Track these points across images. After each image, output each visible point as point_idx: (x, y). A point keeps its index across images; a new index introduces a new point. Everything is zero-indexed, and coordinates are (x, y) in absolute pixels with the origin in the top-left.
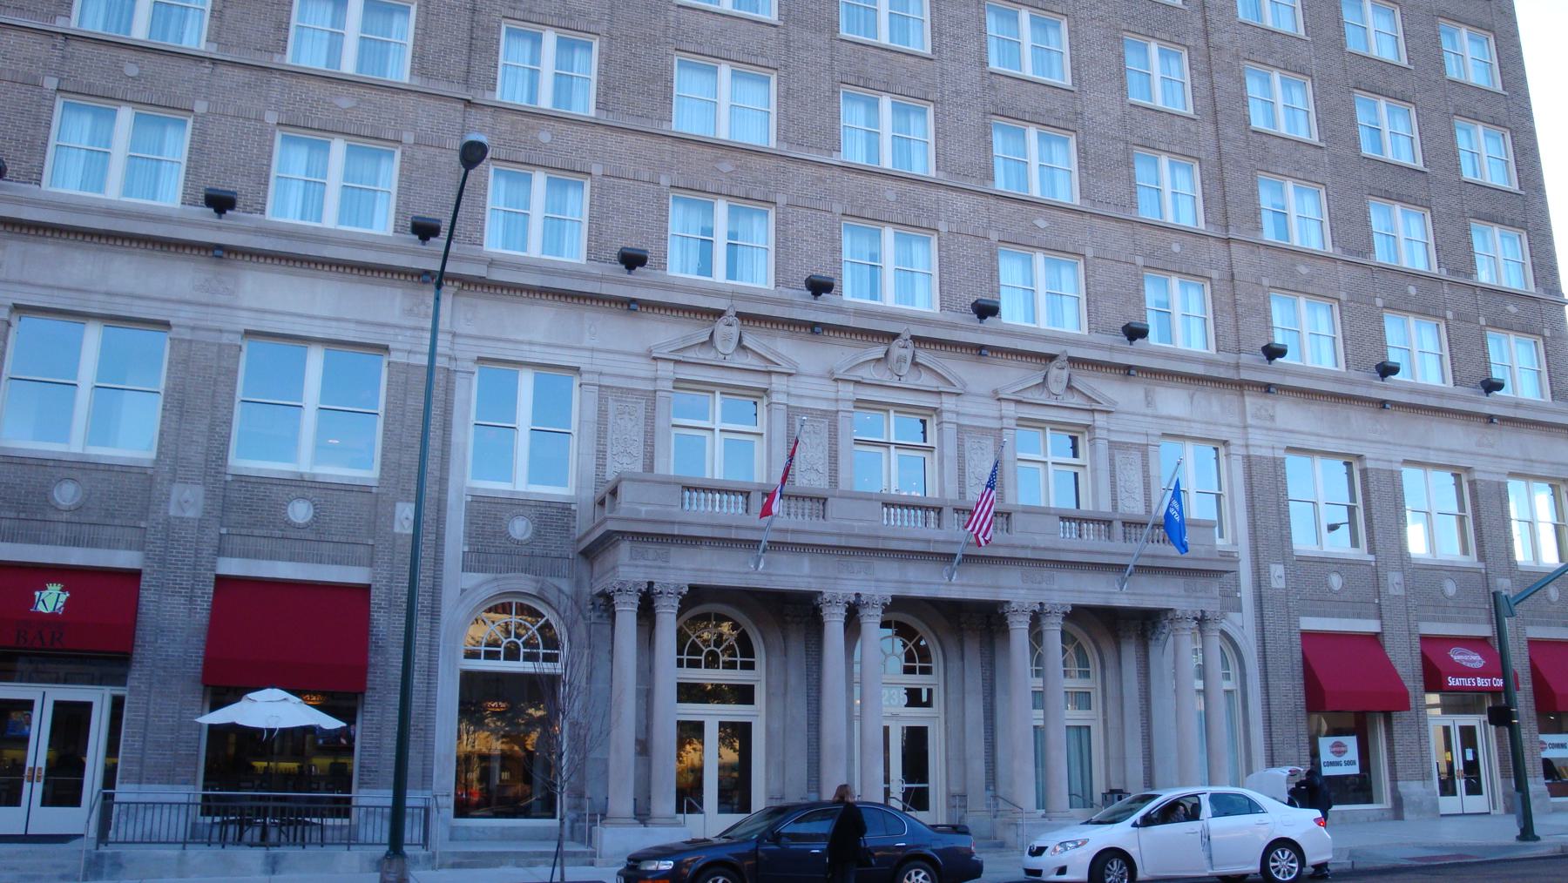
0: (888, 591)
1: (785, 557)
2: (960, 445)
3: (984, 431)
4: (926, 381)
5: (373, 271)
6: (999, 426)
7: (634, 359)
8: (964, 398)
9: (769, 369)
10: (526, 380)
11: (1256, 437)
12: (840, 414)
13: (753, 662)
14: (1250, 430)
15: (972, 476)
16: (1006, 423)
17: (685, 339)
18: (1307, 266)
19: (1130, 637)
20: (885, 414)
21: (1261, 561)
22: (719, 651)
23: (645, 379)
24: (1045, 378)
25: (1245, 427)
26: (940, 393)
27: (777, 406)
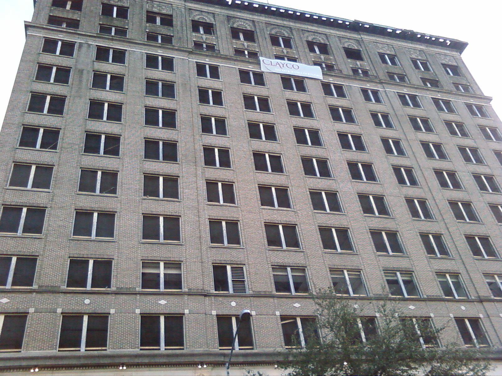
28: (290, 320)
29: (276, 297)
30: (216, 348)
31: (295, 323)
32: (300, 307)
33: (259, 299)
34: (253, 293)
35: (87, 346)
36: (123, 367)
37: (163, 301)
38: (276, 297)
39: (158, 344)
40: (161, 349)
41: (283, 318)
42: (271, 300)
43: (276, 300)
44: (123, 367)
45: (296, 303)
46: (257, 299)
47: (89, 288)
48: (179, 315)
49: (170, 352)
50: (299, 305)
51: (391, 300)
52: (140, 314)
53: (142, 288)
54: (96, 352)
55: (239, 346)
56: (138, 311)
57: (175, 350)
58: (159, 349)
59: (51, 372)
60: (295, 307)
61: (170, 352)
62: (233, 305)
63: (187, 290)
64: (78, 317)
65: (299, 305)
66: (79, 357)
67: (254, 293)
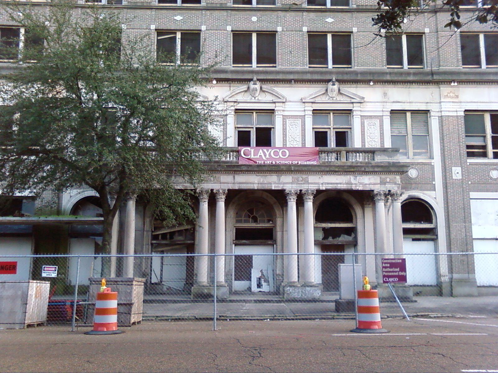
0: (314, 187)
1: (343, 177)
2: (284, 124)
3: (296, 117)
4: (269, 98)
5: (405, 83)
6: (304, 115)
7: (296, 104)
8: (364, 104)
9: (352, 101)
10: (409, 115)
11: (445, 106)
12: (306, 116)
13: (405, 219)
14: (442, 104)
15: (290, 137)
16: (307, 113)
17: (316, 93)
18: (180, 15)
19: (369, 204)
20: (404, 115)
21: (447, 166)
22: (257, 216)
23: (301, 111)
24: (327, 90)
25: (440, 102)
26: (275, 103)
27: (434, 117)
28: (171, 34)
29: (154, 9)
30: (230, 66)
31: (174, 38)
32: (182, 20)
33: (174, 11)
34: (127, 5)
35: (258, 63)
36: (454, 83)
37: (179, 16)
38: (154, 9)
39: (250, 62)
40: (253, 67)
41: (160, 32)
42: (149, 12)
43: (154, 12)
44: (454, 83)
45: (178, 15)
46: (132, 11)
47: (329, 5)
48: (197, 32)
49: (261, 69)
50: (182, 18)
51: (152, 9)
52: (308, 32)
53: (233, 4)
54: (321, 69)
55: (409, 65)
56: (229, 28)
57: (266, 67)
58: (252, 67)
59: (355, 86)
60: (175, 19)
61: (261, 69)
62: (254, 21)
63: (355, 6)
64: (247, 35)
65: (333, 20)
66: (401, 74)
67: (129, 4)
